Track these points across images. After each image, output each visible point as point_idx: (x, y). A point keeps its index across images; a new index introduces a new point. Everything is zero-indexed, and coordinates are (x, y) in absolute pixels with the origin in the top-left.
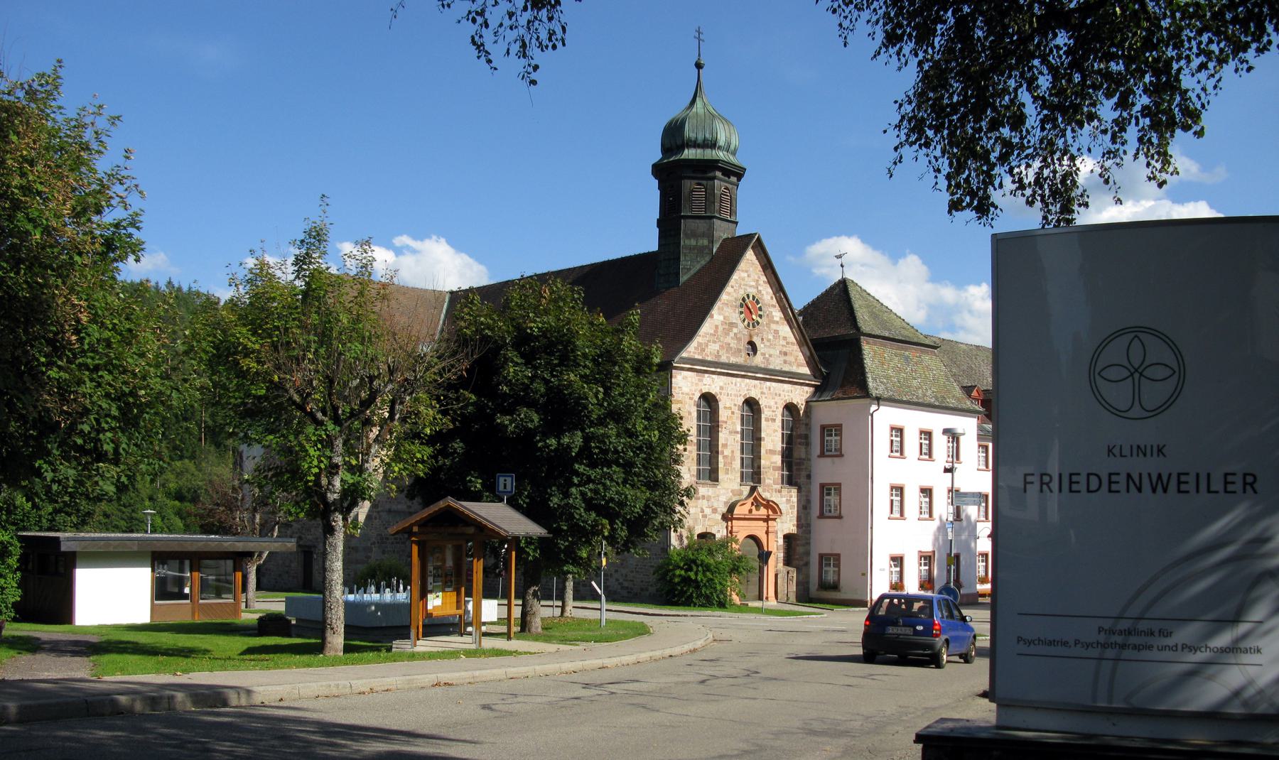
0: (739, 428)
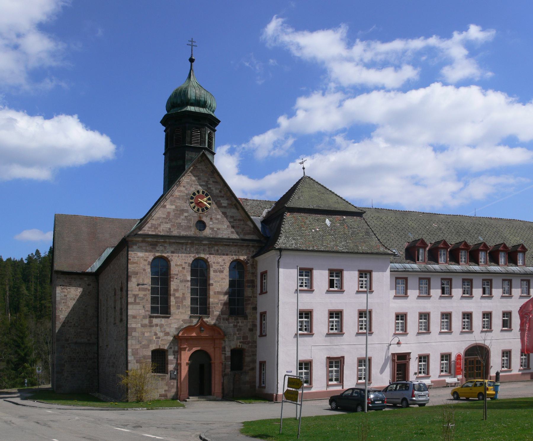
0: (189, 278)
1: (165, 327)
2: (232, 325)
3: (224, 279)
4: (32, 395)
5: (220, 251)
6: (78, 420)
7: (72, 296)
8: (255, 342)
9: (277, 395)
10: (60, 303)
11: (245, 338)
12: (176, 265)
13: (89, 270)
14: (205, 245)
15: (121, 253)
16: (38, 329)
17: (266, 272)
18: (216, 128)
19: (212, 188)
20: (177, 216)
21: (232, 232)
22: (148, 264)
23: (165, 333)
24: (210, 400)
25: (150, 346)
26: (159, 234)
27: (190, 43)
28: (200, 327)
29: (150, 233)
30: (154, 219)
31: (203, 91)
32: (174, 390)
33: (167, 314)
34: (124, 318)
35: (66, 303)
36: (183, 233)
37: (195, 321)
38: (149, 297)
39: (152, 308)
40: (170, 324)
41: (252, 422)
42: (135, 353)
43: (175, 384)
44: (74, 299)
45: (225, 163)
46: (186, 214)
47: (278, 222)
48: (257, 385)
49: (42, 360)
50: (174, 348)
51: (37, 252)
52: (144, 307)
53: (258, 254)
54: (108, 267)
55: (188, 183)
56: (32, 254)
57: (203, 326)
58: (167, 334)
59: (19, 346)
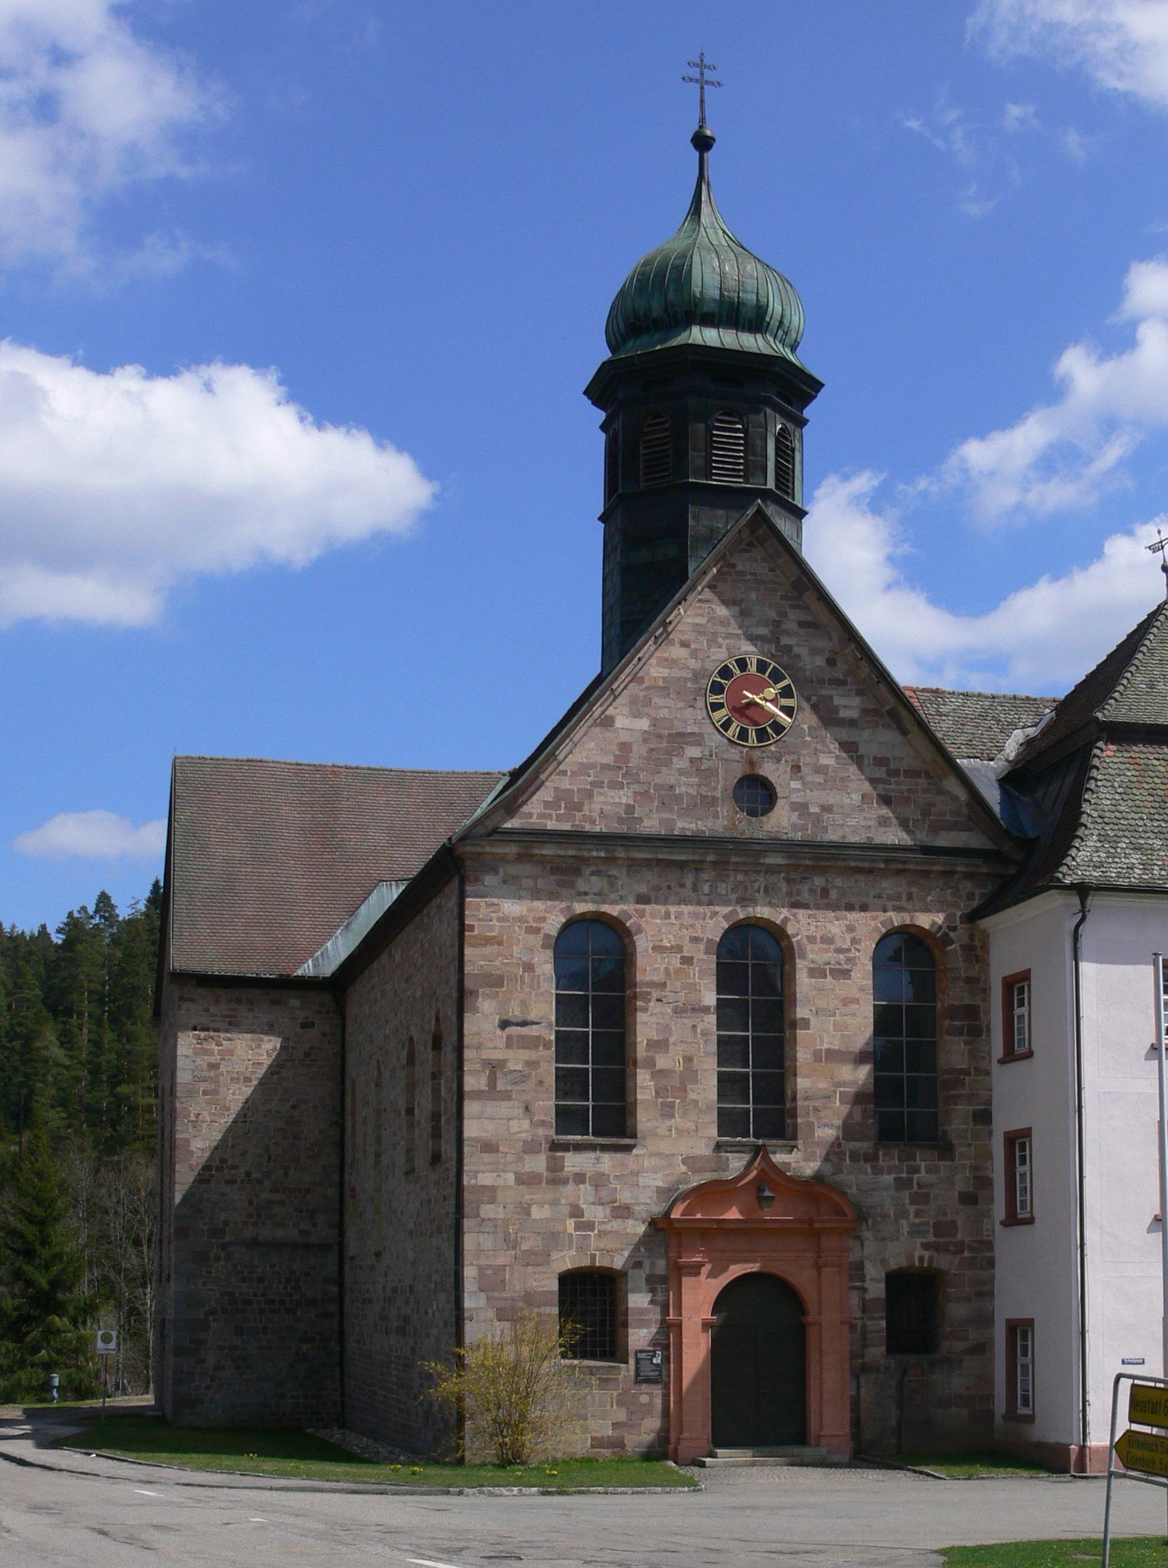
0: (710, 998)
1: (615, 1184)
2: (888, 1179)
3: (856, 1001)
4: (80, 1430)
5: (834, 895)
6: (263, 1527)
7: (240, 1068)
8: (990, 1246)
9: (1083, 1448)
10: (191, 1093)
11: (944, 1228)
12: (658, 949)
13: (307, 969)
14: (772, 870)
15: (435, 903)
16: (103, 1191)
17: (1025, 976)
18: (807, 413)
19: (796, 650)
20: (658, 760)
21: (883, 822)
22: (544, 946)
23: (614, 1209)
24: (802, 1465)
25: (554, 1255)
26: (588, 827)
27: (695, 73)
28: (758, 1186)
29: (551, 825)
30: (565, 773)
31: (750, 267)
32: (651, 1426)
33: (623, 1134)
34: (448, 1150)
35: (216, 1092)
36: (684, 826)
37: (736, 1163)
38: (548, 1069)
39: (561, 1112)
40: (635, 1174)
41: (980, 1548)
42: (491, 1284)
43: (658, 1401)
44: (249, 1080)
45: (843, 544)
46: (693, 752)
47: (1070, 779)
48: (1000, 1407)
49: (119, 1306)
50: (653, 1265)
51: (104, 901)
52: (527, 1109)
53: (992, 905)
54: (384, 958)
55: (701, 630)
56: (84, 909)
57: (768, 1182)
58: (623, 1212)
59: (29, 1254)
